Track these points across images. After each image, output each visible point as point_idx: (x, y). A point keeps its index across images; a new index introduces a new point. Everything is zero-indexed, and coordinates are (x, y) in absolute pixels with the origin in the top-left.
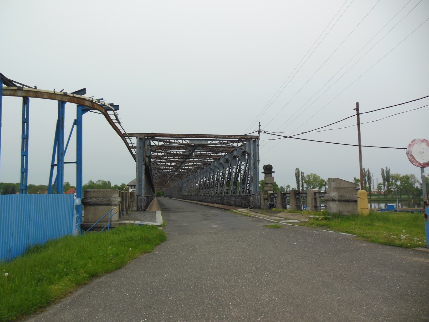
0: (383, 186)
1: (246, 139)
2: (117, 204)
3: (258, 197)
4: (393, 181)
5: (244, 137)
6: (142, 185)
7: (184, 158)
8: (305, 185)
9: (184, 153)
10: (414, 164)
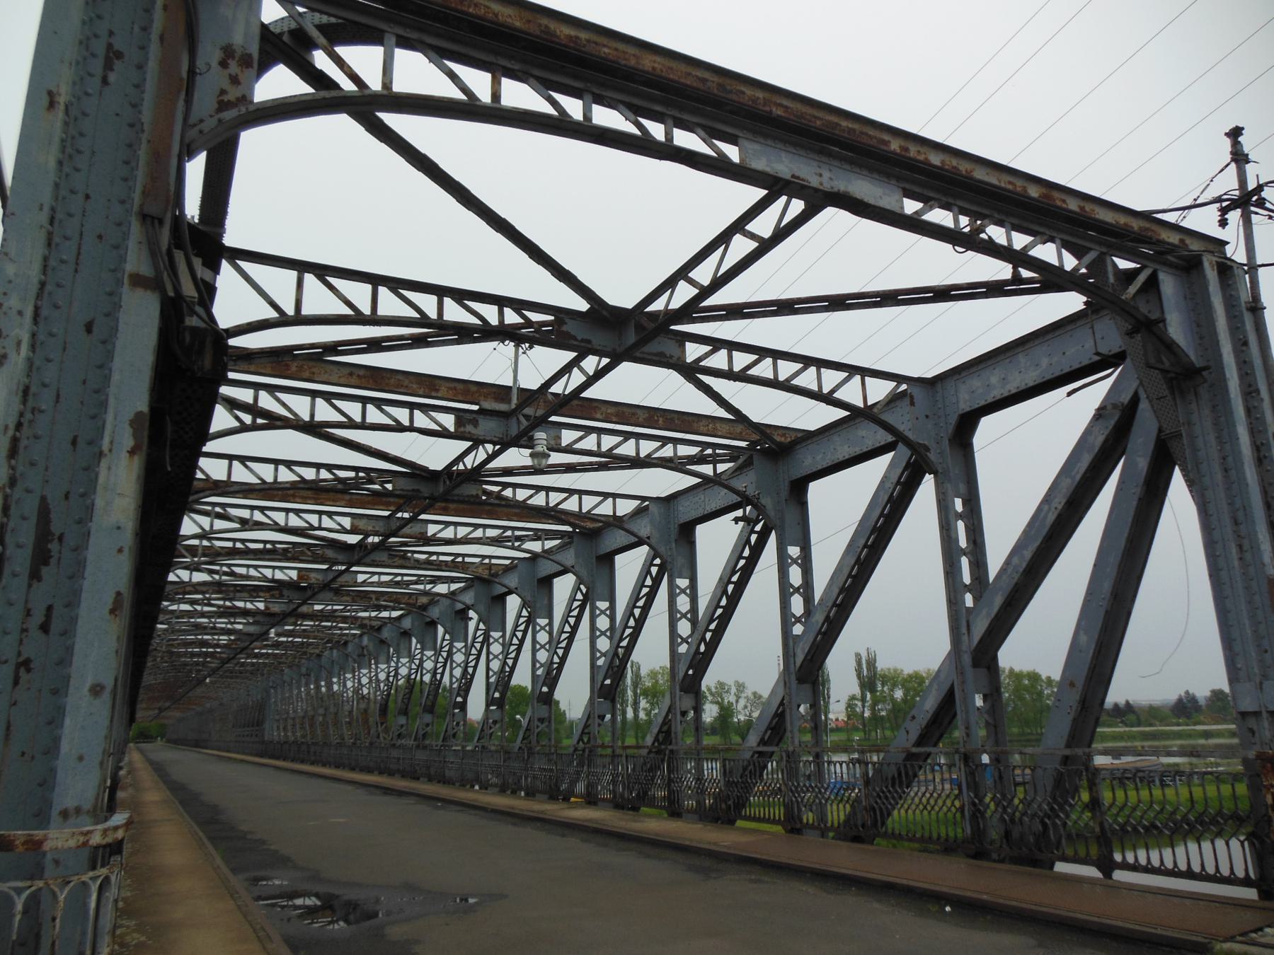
0: (859, 704)
4: (886, 689)
6: (68, 633)
8: (643, 703)
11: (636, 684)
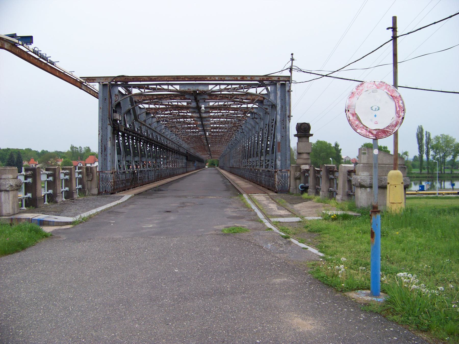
1: (269, 81)
2: (8, 189)
3: (285, 175)
5: (267, 78)
7: (195, 111)
8: (431, 153)
9: (190, 105)
10: (358, 131)
11: (428, 143)
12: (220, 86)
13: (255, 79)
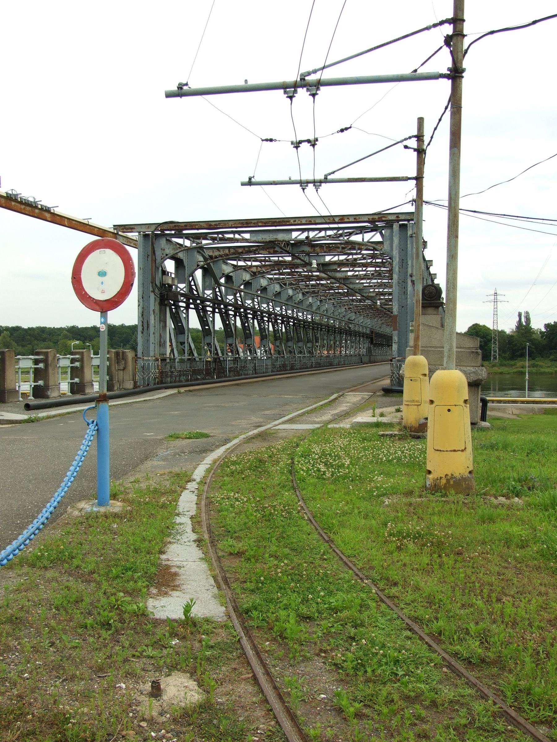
5: (379, 218)
12: (308, 232)
13: (361, 220)
